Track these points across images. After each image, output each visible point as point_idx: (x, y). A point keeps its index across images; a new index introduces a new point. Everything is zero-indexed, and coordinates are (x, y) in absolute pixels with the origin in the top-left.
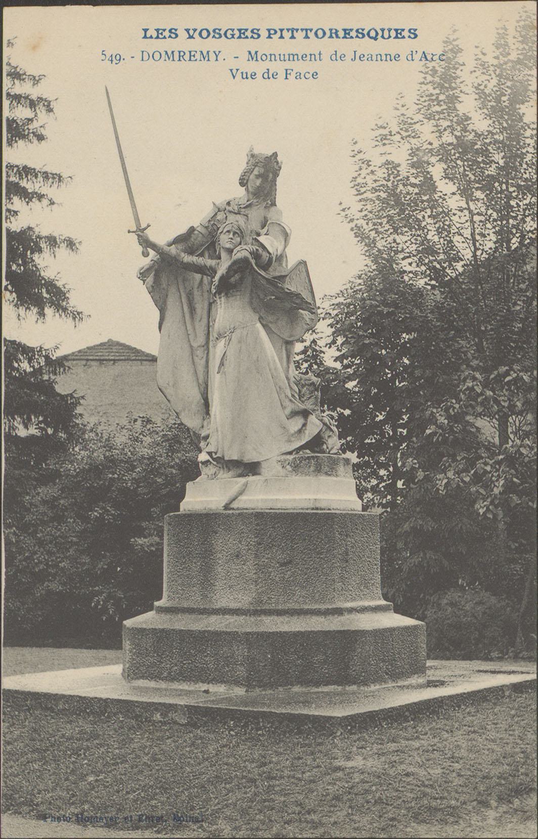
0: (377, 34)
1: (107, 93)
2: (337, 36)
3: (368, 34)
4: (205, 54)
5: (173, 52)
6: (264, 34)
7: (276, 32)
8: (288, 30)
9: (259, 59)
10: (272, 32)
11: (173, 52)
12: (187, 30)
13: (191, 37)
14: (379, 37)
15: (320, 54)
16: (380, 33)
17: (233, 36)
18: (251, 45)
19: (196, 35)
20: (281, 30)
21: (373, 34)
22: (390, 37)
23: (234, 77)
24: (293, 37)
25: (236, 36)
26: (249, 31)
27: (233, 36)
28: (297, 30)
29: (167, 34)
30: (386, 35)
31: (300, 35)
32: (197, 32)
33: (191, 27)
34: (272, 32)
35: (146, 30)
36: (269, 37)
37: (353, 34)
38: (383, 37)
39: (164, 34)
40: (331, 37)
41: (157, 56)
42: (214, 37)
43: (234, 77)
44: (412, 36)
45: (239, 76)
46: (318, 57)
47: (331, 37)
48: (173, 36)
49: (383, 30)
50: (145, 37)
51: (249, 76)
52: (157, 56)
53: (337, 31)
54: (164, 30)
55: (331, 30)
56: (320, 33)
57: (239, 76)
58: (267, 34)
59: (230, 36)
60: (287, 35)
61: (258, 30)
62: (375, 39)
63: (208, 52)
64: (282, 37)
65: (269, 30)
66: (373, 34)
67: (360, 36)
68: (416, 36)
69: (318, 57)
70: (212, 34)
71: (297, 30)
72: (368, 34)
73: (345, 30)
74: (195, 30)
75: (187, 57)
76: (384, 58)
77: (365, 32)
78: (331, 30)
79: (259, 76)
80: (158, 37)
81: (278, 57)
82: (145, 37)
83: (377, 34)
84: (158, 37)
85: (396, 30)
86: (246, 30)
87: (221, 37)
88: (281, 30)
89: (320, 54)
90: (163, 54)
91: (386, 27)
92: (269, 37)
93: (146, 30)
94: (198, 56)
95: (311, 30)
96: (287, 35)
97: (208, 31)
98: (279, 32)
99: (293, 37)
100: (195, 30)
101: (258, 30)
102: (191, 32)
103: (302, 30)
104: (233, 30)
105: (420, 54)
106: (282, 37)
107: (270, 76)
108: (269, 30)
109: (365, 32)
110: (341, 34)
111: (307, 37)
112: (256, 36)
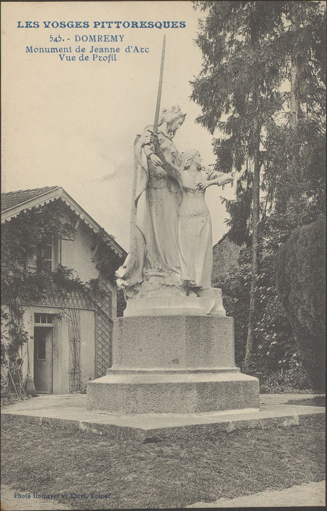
0: (161, 25)
1: (164, 41)
2: (137, 27)
3: (156, 25)
4: (114, 37)
5: (94, 36)
6: (92, 25)
7: (99, 24)
8: (107, 23)
9: (33, 50)
10: (97, 24)
11: (94, 36)
12: (45, 23)
13: (47, 27)
14: (162, 26)
15: (70, 48)
16: (163, 24)
17: (72, 26)
18: (82, 32)
19: (50, 25)
20: (103, 23)
21: (158, 25)
22: (169, 26)
23: (62, 59)
24: (110, 27)
25: (74, 26)
26: (179, 23)
27: (72, 26)
28: (112, 23)
29: (178, 25)
30: (167, 26)
31: (114, 26)
32: (51, 24)
33: (47, 21)
34: (97, 24)
35: (19, 23)
36: (95, 27)
37: (82, 25)
38: (165, 26)
39: (146, 24)
40: (133, 27)
41: (85, 38)
42: (61, 27)
43: (62, 59)
44: (182, 26)
45: (65, 59)
46: (69, 50)
47: (133, 27)
48: (86, 26)
49: (165, 23)
50: (19, 27)
51: (71, 59)
52: (85, 38)
53: (137, 23)
54: (146, 22)
55: (133, 22)
56: (126, 25)
57: (65, 59)
58: (94, 25)
59: (70, 26)
60: (106, 25)
61: (184, 22)
62: (160, 28)
63: (116, 36)
64: (103, 27)
65: (95, 23)
66: (158, 25)
67: (151, 26)
68: (185, 26)
69: (69, 50)
70: (60, 25)
71: (112, 23)
72: (156, 25)
73: (141, 23)
74: (49, 22)
75: (103, 39)
76: (104, 50)
77: (154, 24)
78: (133, 22)
79: (77, 58)
80: (27, 27)
81: (44, 50)
82: (19, 27)
83: (161, 25)
84: (27, 27)
85: (173, 23)
86: (31, 22)
87: (153, 26)
88: (103, 23)
89: (70, 48)
90: (89, 37)
91: (167, 21)
92: (95, 27)
93: (19, 23)
94: (110, 38)
95: (121, 22)
96: (106, 25)
97: (57, 23)
98: (101, 24)
99: (110, 27)
100: (49, 22)
101: (184, 22)
102: (47, 24)
103: (115, 23)
104: (72, 22)
105: (134, 48)
106: (103, 27)
107: (84, 58)
108: (95, 23)
109: (154, 24)
110: (139, 25)
111: (118, 27)
112: (86, 26)
